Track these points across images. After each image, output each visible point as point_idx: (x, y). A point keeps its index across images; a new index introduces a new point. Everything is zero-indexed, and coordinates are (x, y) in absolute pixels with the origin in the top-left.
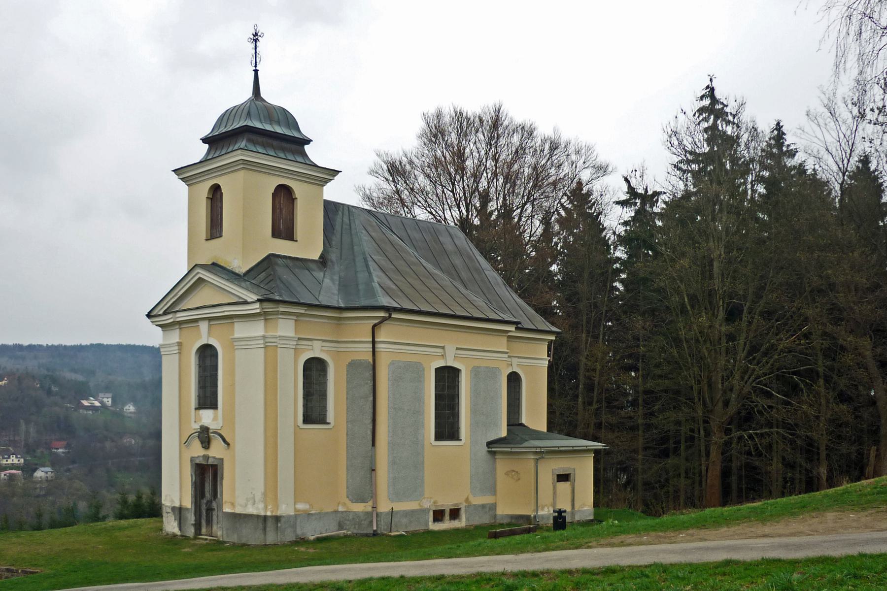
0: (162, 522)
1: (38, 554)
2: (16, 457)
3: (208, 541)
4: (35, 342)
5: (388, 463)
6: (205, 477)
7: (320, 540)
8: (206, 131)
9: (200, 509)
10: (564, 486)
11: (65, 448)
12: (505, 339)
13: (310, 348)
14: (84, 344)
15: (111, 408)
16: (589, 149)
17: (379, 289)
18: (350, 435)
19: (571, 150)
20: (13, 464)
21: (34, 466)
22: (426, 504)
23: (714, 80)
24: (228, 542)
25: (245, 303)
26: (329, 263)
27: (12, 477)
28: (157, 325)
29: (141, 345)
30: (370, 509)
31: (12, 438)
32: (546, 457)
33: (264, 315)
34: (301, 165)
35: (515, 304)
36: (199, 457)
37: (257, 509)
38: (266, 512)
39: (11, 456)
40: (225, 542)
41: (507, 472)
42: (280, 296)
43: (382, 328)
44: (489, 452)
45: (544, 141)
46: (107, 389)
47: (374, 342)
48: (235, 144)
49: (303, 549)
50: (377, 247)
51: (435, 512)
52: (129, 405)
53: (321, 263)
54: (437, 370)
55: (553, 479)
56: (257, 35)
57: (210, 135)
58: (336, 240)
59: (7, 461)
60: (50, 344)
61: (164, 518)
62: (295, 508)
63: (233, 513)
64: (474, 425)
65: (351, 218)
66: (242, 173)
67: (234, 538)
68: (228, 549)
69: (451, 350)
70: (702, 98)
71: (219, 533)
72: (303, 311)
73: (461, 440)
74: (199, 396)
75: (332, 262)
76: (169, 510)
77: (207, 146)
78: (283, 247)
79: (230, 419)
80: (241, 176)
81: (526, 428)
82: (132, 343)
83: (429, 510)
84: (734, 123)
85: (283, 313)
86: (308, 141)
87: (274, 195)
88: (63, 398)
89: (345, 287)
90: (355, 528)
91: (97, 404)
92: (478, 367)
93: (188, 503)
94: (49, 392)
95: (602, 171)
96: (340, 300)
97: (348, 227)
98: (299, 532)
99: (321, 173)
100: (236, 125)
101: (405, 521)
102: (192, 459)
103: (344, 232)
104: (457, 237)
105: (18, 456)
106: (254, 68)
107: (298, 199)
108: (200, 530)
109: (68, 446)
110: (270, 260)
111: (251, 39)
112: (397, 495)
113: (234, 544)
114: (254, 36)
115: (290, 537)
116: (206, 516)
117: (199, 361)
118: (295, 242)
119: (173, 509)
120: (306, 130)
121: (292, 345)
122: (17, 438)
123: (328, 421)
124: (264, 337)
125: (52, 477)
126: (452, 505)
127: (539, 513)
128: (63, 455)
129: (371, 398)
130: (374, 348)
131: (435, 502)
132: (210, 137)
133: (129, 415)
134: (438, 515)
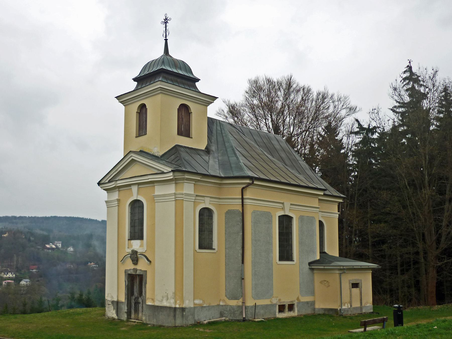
0: (105, 310)
1: (29, 330)
2: (11, 274)
3: (136, 323)
4: (22, 215)
5: (252, 275)
6: (133, 283)
7: (210, 324)
8: (136, 74)
9: (131, 303)
10: (356, 291)
11: (37, 269)
12: (317, 200)
13: (203, 201)
14: (48, 216)
15: (61, 249)
16: (345, 98)
17: (245, 167)
18: (227, 256)
19: (335, 98)
20: (9, 277)
21: (21, 278)
22: (275, 301)
23: (411, 62)
24: (150, 324)
25: (163, 173)
26: (212, 152)
27: (9, 284)
28: (104, 189)
29: (77, 217)
30: (240, 304)
31: (9, 264)
32: (346, 272)
33: (175, 181)
34: (194, 93)
35: (318, 180)
36: (130, 270)
37: (170, 303)
38: (176, 305)
39: (9, 273)
40: (148, 324)
41: (322, 281)
42: (186, 168)
43: (247, 189)
44: (310, 269)
45: (319, 94)
46: (59, 240)
47: (243, 199)
48: (155, 80)
49: (201, 330)
50: (238, 142)
51: (279, 306)
52: (70, 247)
53: (206, 151)
54: (279, 217)
55: (350, 286)
56: (167, 20)
57: (139, 76)
58: (214, 139)
59: (6, 275)
60: (30, 216)
61: (106, 308)
62: (194, 303)
63: (153, 305)
64: (301, 252)
65: (222, 127)
66: (160, 95)
67: (154, 322)
68: (150, 328)
69: (287, 205)
70: (405, 72)
71: (144, 318)
72: (199, 179)
73: (294, 261)
74: (131, 232)
75: (212, 151)
76: (110, 303)
77: (136, 83)
78: (183, 141)
79: (151, 245)
80: (159, 97)
81: (326, 254)
82: (72, 216)
83: (276, 304)
84: (424, 86)
85: (188, 179)
86: (198, 80)
87: (179, 110)
88: (36, 243)
89: (222, 165)
90: (231, 316)
91: (54, 246)
92: (303, 216)
93: (123, 298)
94: (29, 240)
95: (352, 111)
96: (220, 173)
97: (220, 132)
98: (196, 318)
99: (208, 98)
100: (155, 69)
101: (262, 312)
102: (126, 271)
103: (218, 135)
104: (281, 141)
105: (12, 273)
106: (165, 38)
107: (193, 113)
108: (130, 316)
109: (38, 268)
110: (177, 148)
111: (163, 22)
112: (257, 296)
113: (154, 325)
114: (165, 20)
115: (191, 321)
116: (135, 307)
117: (131, 210)
118: (191, 139)
119: (113, 302)
120: (196, 73)
121: (192, 199)
122: (12, 264)
123: (213, 248)
124: (175, 194)
125: (29, 284)
126: (289, 302)
127: (342, 308)
128: (36, 273)
129: (241, 234)
130: (243, 202)
131: (280, 300)
132: (139, 77)
133: (70, 253)
134: (282, 308)
